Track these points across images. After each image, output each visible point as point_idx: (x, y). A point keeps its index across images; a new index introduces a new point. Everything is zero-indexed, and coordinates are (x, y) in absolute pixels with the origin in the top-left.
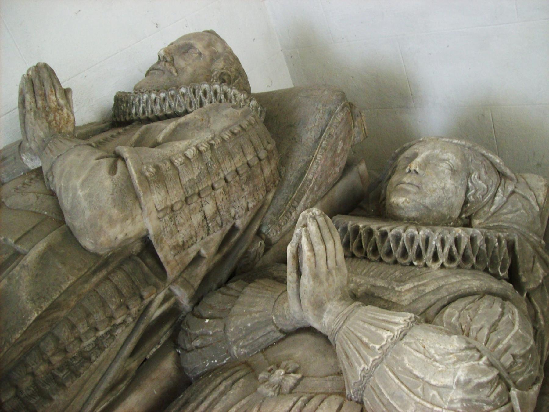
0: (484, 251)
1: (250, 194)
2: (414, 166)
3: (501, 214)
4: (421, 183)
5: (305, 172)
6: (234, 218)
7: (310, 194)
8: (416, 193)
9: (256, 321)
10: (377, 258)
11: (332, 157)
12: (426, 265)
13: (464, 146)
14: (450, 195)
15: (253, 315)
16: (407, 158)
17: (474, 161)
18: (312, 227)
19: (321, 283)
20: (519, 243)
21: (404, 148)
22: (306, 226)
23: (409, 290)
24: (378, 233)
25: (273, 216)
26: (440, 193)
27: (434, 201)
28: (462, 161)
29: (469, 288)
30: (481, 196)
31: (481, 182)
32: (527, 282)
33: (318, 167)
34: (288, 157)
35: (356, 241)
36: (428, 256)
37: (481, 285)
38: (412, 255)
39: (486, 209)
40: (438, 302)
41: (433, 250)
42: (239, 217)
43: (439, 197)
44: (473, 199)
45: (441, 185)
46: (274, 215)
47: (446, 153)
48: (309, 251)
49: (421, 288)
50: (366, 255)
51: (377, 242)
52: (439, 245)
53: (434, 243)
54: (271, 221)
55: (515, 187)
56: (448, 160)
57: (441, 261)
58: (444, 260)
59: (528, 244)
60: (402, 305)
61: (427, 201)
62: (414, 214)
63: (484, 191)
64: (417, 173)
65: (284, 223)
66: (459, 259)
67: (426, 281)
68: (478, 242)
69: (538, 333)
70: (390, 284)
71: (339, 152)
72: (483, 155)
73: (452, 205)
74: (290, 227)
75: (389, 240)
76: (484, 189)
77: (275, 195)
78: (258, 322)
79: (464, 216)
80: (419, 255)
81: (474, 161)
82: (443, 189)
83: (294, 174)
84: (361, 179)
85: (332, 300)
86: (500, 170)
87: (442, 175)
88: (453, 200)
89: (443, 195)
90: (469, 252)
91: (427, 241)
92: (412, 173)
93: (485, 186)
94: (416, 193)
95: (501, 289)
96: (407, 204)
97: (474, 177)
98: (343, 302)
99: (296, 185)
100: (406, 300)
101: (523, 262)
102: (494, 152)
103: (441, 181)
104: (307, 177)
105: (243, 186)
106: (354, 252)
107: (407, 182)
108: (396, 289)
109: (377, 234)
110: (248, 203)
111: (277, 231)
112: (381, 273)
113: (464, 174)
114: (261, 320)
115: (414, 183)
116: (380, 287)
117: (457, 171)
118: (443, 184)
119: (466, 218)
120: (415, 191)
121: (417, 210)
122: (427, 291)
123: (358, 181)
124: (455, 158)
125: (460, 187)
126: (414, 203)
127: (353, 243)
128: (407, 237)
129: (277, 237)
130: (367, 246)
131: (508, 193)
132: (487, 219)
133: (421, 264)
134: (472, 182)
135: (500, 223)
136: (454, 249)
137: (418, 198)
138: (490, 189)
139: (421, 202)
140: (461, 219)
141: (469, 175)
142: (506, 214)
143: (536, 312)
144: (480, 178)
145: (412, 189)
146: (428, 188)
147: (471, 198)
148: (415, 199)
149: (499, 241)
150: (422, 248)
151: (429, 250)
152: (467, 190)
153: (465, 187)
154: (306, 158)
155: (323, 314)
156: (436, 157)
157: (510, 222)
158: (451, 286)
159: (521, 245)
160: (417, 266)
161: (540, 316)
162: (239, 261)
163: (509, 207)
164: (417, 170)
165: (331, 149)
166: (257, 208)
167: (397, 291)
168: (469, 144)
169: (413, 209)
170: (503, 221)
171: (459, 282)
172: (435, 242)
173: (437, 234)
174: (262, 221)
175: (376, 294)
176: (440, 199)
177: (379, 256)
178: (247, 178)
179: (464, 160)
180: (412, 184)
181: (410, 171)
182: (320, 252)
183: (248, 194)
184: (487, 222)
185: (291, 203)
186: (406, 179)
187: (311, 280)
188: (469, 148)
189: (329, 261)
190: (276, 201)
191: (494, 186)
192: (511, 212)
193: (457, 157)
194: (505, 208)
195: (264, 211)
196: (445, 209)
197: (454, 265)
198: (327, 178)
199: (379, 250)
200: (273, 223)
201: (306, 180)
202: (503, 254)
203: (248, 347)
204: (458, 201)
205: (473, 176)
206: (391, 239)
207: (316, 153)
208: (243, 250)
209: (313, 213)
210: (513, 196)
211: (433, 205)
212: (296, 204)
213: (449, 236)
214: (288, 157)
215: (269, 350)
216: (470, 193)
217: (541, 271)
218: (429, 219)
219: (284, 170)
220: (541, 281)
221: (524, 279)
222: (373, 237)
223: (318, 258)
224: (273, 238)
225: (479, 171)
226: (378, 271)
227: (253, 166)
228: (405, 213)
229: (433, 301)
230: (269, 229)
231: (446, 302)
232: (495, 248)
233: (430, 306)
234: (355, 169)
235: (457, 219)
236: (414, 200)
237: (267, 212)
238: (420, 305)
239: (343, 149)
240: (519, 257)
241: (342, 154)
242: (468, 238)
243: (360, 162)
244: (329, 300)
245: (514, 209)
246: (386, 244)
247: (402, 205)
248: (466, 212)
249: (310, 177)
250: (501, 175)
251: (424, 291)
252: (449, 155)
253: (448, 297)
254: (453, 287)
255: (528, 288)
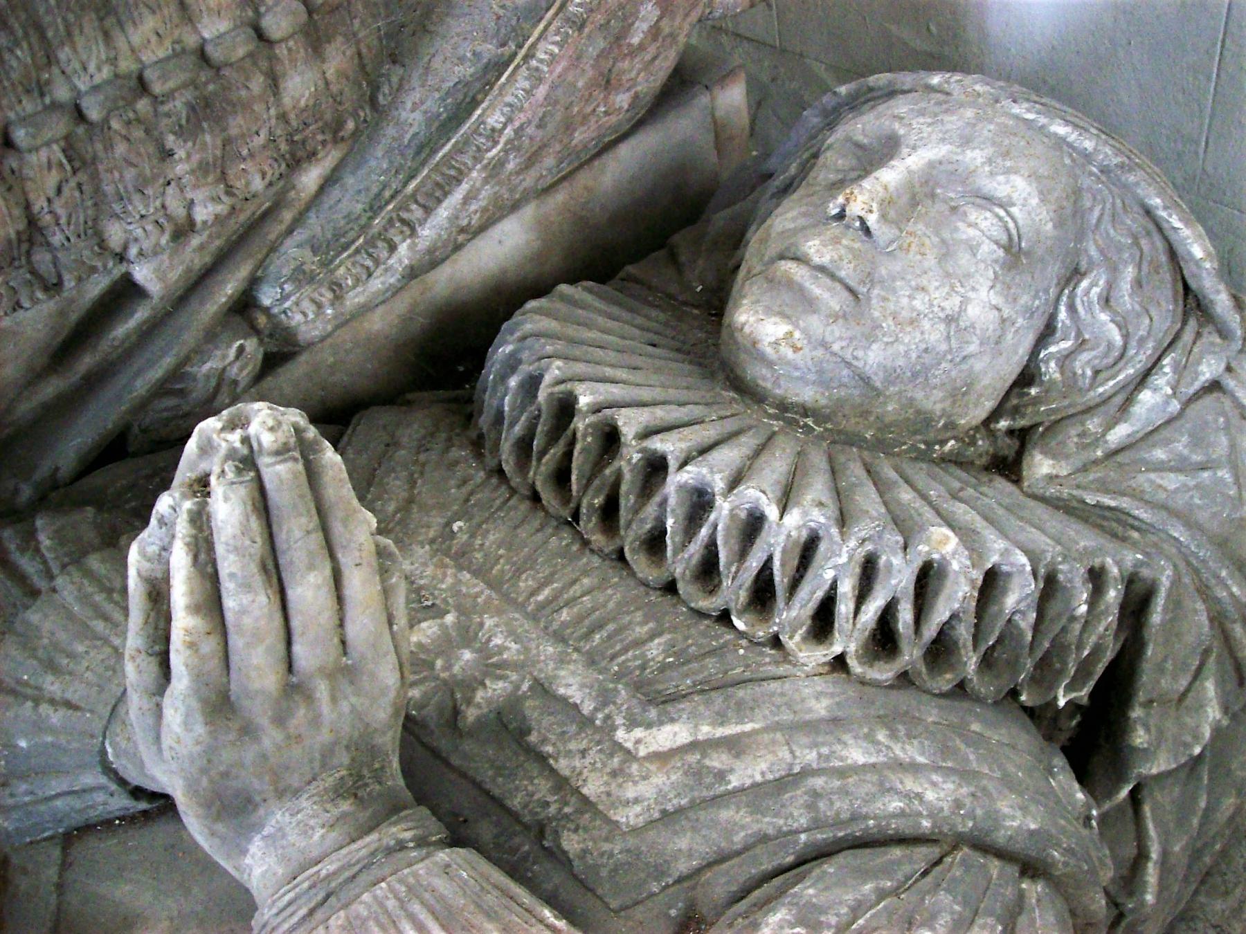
0: (1021, 633)
1: (203, 169)
2: (862, 200)
3: (1145, 462)
4: (870, 278)
5: (475, 103)
6: (121, 257)
7: (486, 181)
8: (835, 317)
9: (49, 739)
10: (610, 548)
11: (602, 55)
12: (776, 642)
13: (1087, 157)
14: (973, 348)
15: (45, 709)
16: (858, 146)
17: (1106, 224)
18: (228, 509)
19: (248, 731)
20: (1168, 596)
21: (871, 89)
22: (202, 485)
23: (662, 757)
24: (636, 457)
25: (307, 253)
26: (934, 334)
27: (901, 362)
28: (1059, 224)
29: (902, 814)
30: (1089, 373)
31: (1108, 317)
32: (1145, 750)
33: (534, 87)
34: (426, 31)
35: (556, 452)
36: (793, 614)
37: (958, 804)
38: (735, 587)
39: (1093, 425)
40: (758, 850)
41: (820, 594)
42: (141, 253)
43: (926, 350)
44: (1057, 376)
45: (945, 304)
46: (315, 251)
47: (1008, 171)
48: (195, 609)
49: (717, 761)
50: (576, 515)
51: (624, 488)
52: (847, 588)
53: (829, 575)
54: (299, 269)
55: (1229, 369)
56: (1005, 204)
57: (837, 649)
58: (852, 648)
59: (1200, 606)
60: (616, 824)
61: (873, 358)
62: (807, 394)
63: (1106, 355)
64: (867, 231)
65: (357, 281)
66: (911, 654)
67: (748, 727)
68: (1011, 601)
69: (1123, 924)
70: (605, 698)
71: (636, 40)
72: (1148, 212)
73: (969, 385)
74: (378, 293)
75: (664, 502)
76: (1110, 345)
77: (336, 169)
78: (53, 745)
79: (1003, 424)
80: (763, 594)
81: (1106, 224)
82: (950, 320)
83: (429, 103)
84: (717, 136)
85: (296, 793)
86: (1193, 284)
87: (964, 259)
88: (978, 366)
89: (944, 347)
90: (963, 633)
91: (808, 550)
92: (848, 227)
93: (1118, 339)
94: (835, 317)
95: (1032, 833)
96: (789, 354)
97: (1087, 293)
98: (346, 806)
99: (425, 148)
100: (636, 801)
101: (1161, 670)
102: (1198, 215)
103: (952, 288)
104: (481, 121)
105: (170, 141)
106: (539, 487)
107: (817, 260)
108: (620, 735)
109: (631, 455)
110: (192, 202)
111: (319, 306)
112: (600, 626)
113: (1054, 270)
114: (63, 740)
115: (842, 274)
116: (564, 700)
117: (1028, 254)
118: (957, 300)
119: (1010, 432)
120: (835, 305)
121: (823, 382)
122: (734, 782)
123: (706, 141)
124: (1034, 201)
125: (1020, 321)
126: (819, 353)
127: (543, 453)
128: (733, 515)
129: (319, 325)
130: (589, 481)
131: (1197, 385)
132: (1084, 469)
133: (761, 634)
134: (1072, 308)
135: (1124, 503)
136: (905, 615)
137: (836, 334)
138: (1132, 352)
139: (849, 357)
140: (992, 434)
141: (1074, 274)
142: (1160, 467)
143: (1142, 856)
144: (1106, 301)
145: (826, 295)
146: (891, 306)
147: (1051, 370)
148: (829, 339)
149: (1096, 577)
150: (780, 579)
151: (804, 592)
152: (1047, 333)
153: (1039, 323)
154: (489, 49)
155: (250, 840)
156: (962, 177)
157: (1164, 507)
158: (837, 783)
159: (1175, 604)
160: (742, 635)
161: (1152, 874)
162: (143, 405)
163: (1181, 445)
164: (872, 220)
165: (604, 27)
166: (234, 225)
167: (619, 747)
168: (1108, 154)
169: (812, 377)
170: (1138, 496)
171: (874, 765)
172: (836, 567)
173: (853, 543)
174: (261, 264)
175: (533, 738)
176: (927, 359)
177: (618, 542)
178: (192, 108)
179: (1072, 216)
180: (833, 277)
181: (841, 216)
182: (247, 621)
183: (193, 172)
184: (1081, 478)
185: (398, 209)
186: (816, 248)
187: (199, 717)
188: (1105, 170)
189: (297, 648)
190: (336, 192)
191: (1150, 345)
192: (1181, 466)
193: (1044, 197)
194: (1167, 442)
195: (274, 230)
196: (938, 394)
197: (884, 672)
198: (569, 127)
199: (622, 522)
200: (302, 277)
201: (476, 131)
202: (1093, 639)
203: (15, 815)
204: (992, 374)
205: (1084, 284)
206: (672, 501)
207: (536, 34)
208: (156, 373)
209: (246, 440)
210: (1208, 400)
211: (892, 376)
212: (417, 212)
213: (897, 561)
214: (426, 31)
215: (92, 842)
216: (1053, 349)
217: (1213, 712)
218: (856, 436)
219: (395, 79)
220: (1197, 750)
221: (1140, 738)
222: (616, 464)
223: (236, 641)
224: (303, 328)
225: (1114, 270)
226: (594, 609)
227: (228, 65)
228: (776, 383)
229: (739, 838)
230: (284, 298)
231: (790, 859)
232: (1073, 619)
233: (722, 858)
234: (704, 99)
235: (977, 429)
236: (824, 345)
237: (290, 231)
238: (683, 843)
239: (655, 32)
240: (1145, 678)
241: (652, 50)
242: (973, 581)
243: (726, 77)
244: (284, 793)
245: (1197, 458)
246: (651, 510)
247: (769, 351)
248: (1016, 412)
249: (495, 119)
250: (1191, 301)
251: (721, 776)
252: (1018, 189)
253: (803, 837)
254: (844, 792)
255: (1144, 771)
